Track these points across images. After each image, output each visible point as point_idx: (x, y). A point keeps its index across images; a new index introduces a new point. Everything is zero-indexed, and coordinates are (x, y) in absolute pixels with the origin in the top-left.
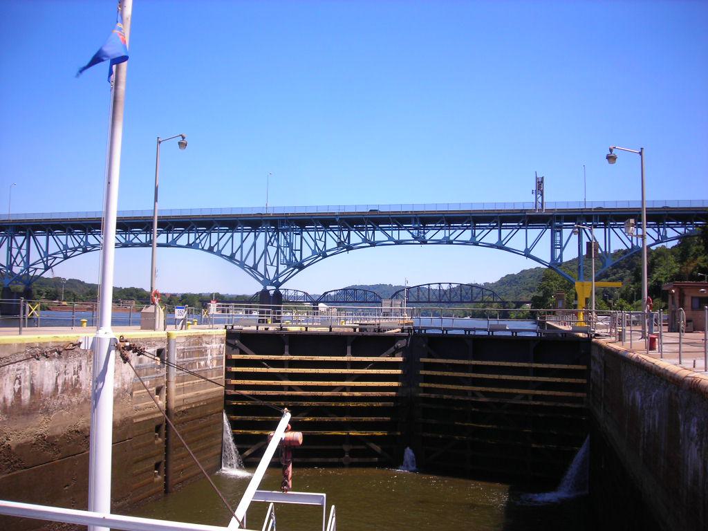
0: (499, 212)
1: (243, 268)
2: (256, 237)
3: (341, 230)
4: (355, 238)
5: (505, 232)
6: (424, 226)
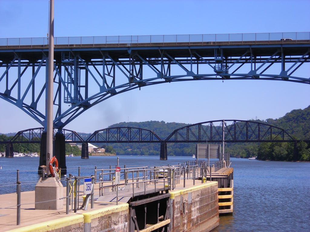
0: (220, 44)
1: (21, 107)
2: (34, 74)
3: (133, 64)
4: (148, 72)
5: (288, 65)
6: (198, 59)
